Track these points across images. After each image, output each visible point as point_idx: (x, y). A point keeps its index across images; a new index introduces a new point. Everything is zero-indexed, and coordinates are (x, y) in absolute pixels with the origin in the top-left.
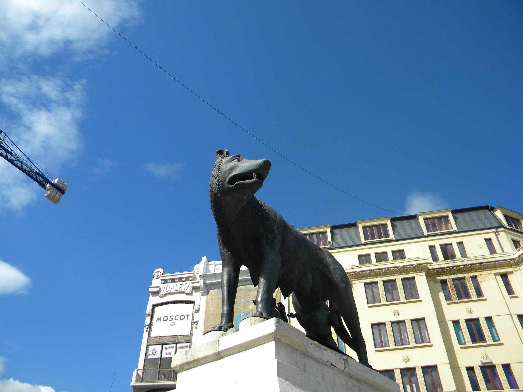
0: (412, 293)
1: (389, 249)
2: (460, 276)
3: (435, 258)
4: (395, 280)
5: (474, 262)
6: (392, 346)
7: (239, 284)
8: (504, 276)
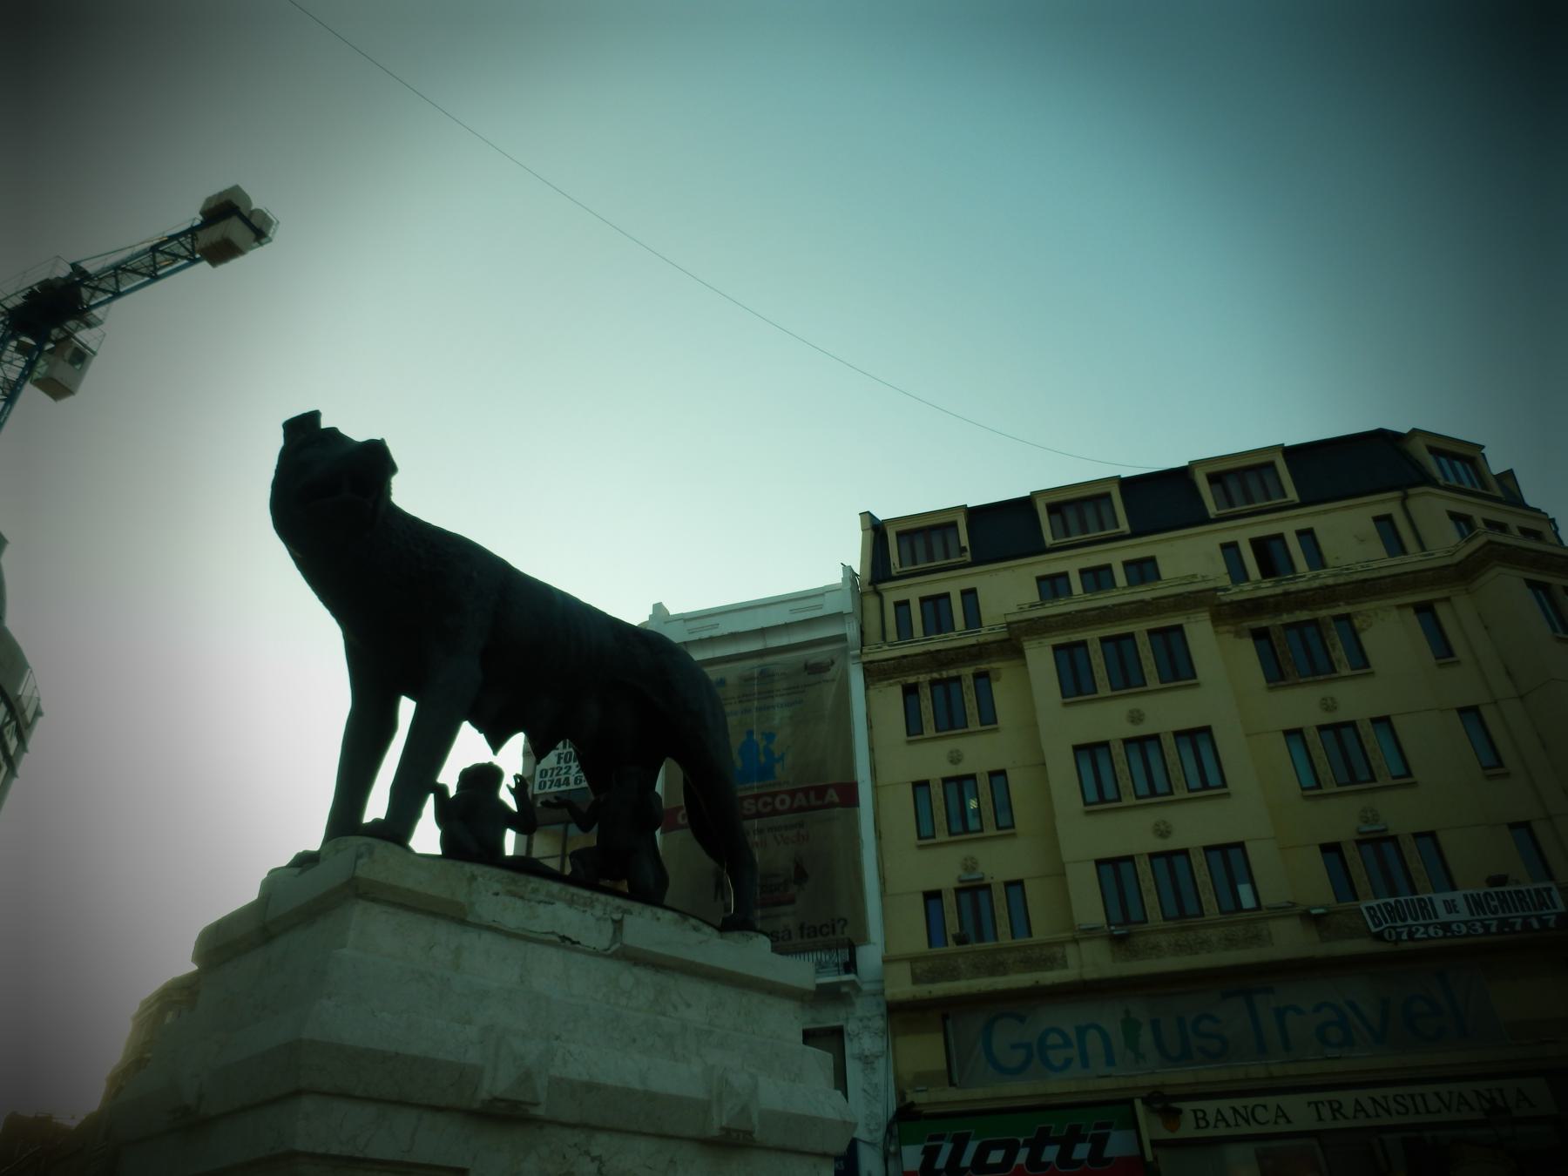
0: (1178, 667)
1: (1115, 556)
2: (1304, 615)
3: (1237, 572)
4: (1083, 644)
5: (1341, 580)
8: (1425, 610)
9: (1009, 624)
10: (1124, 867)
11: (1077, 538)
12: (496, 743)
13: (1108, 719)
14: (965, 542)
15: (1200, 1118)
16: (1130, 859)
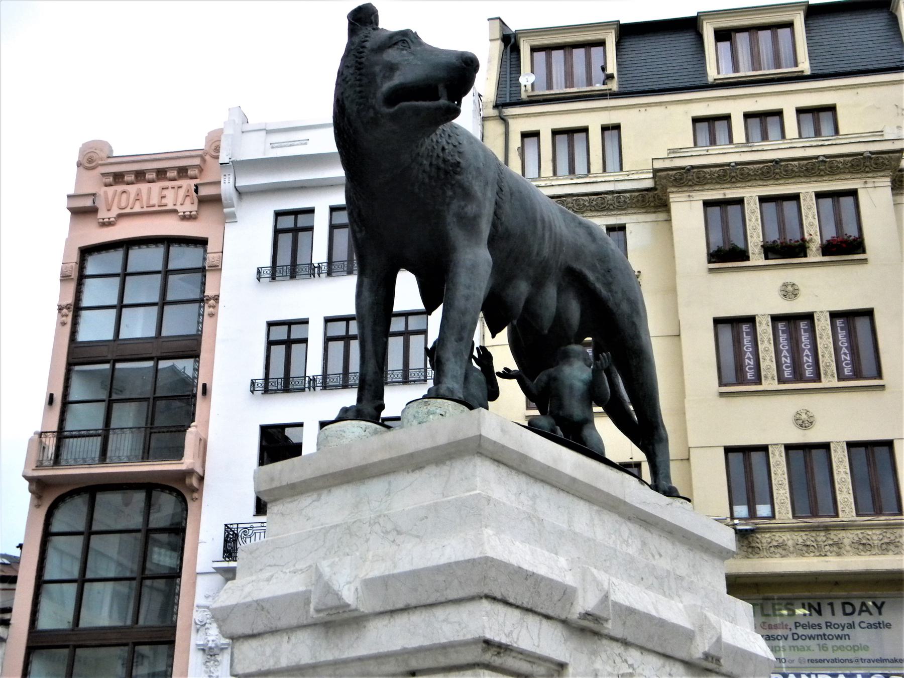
1: (788, 101)
6: (770, 383)
7: (344, 181)
9: (656, 171)
10: (756, 457)
12: (494, 333)
13: (758, 291)
14: (612, 68)
16: (764, 449)
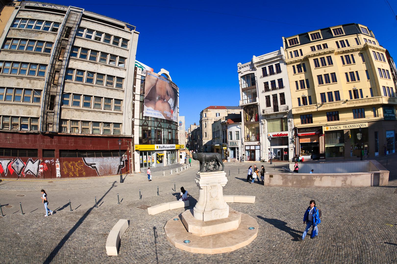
1: (321, 43)
11: (317, 39)
15: (331, 128)
